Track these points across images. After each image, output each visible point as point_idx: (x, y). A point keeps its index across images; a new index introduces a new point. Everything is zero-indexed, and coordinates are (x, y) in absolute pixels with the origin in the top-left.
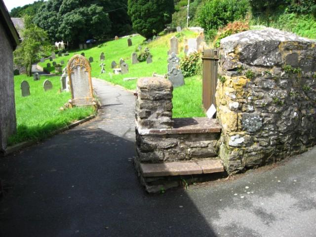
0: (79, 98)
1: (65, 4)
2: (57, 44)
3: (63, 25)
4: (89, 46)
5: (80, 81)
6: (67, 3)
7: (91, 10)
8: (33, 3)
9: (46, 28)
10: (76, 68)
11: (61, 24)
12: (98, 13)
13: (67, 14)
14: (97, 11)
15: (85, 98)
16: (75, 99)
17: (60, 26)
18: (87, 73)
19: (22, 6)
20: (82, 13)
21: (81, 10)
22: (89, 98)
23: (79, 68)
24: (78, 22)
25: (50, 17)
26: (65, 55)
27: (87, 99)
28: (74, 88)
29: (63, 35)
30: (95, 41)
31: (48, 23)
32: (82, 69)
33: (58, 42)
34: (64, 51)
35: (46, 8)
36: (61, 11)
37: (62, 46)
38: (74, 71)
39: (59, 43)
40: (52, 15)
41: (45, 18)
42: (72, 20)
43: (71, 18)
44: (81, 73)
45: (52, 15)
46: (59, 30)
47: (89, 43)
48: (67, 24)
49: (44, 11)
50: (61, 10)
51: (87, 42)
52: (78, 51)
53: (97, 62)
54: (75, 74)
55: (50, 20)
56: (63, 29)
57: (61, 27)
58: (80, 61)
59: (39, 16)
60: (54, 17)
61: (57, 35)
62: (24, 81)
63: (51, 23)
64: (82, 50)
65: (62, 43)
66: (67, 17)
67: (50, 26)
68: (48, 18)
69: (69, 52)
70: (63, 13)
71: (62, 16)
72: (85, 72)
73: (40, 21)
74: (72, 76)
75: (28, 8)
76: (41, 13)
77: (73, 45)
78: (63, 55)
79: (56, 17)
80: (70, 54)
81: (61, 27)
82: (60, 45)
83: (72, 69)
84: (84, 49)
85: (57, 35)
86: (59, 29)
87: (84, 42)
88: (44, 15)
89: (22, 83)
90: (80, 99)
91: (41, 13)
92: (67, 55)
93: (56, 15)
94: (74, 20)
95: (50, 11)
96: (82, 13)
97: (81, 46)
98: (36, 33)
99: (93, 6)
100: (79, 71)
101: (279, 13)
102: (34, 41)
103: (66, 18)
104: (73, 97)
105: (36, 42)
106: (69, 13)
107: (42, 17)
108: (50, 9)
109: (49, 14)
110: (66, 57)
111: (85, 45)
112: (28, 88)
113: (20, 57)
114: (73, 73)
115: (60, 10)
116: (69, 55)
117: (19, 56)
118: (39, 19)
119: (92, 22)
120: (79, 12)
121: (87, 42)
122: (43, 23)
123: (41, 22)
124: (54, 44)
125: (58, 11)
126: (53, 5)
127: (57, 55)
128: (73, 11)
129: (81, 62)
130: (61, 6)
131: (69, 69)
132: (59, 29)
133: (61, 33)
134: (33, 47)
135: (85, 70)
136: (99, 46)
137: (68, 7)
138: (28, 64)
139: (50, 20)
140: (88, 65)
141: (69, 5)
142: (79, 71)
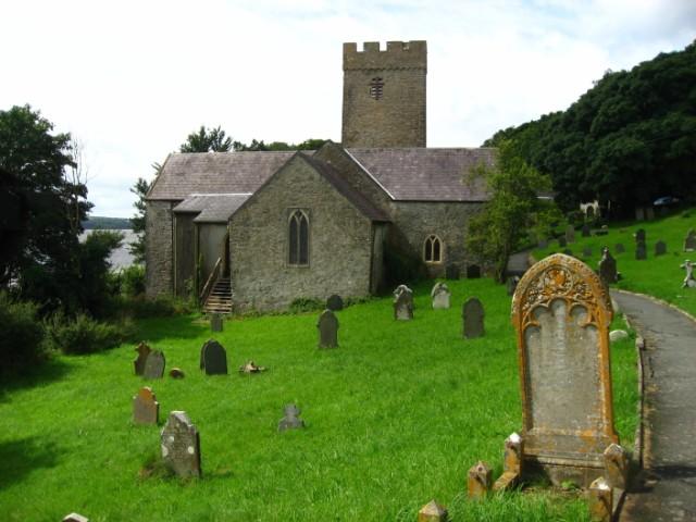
0: (555, 430)
1: (605, 114)
2: (584, 207)
3: (597, 163)
4: (660, 214)
5: (560, 363)
6: (610, 112)
7: (669, 125)
8: (539, 118)
9: (558, 169)
10: (550, 310)
11: (594, 160)
12: (688, 133)
13: (608, 137)
14: (684, 128)
15: (578, 433)
16: (537, 430)
17: (589, 165)
18: (592, 333)
19: (517, 125)
20: (644, 134)
21: (644, 126)
22: (592, 434)
23: (561, 311)
24: (635, 155)
25: (568, 145)
26: (598, 234)
27: (586, 440)
28: (534, 386)
29: (595, 187)
30: (675, 200)
31: (563, 157)
32: (571, 313)
33: (585, 203)
34: (597, 225)
35: (560, 126)
36: (594, 132)
37: (595, 212)
38: (542, 320)
39: (589, 204)
40: (573, 141)
41: (558, 148)
42: (620, 151)
43: (617, 147)
44: (569, 329)
45: (573, 141)
46: (588, 175)
47: (660, 206)
48: (607, 159)
49: (556, 132)
50: (595, 128)
51: (656, 203)
52: (630, 225)
53: (676, 254)
54: (544, 331)
55: (567, 151)
56: (596, 171)
57: (593, 167)
58: (565, 281)
59: (545, 143)
60: (577, 145)
61: (581, 187)
62: (472, 300)
63: (570, 157)
64: (641, 222)
65: (595, 205)
66: (608, 144)
67: (568, 165)
68: (564, 147)
69: (609, 226)
70: (599, 135)
71: (597, 144)
72: (586, 327)
73: (545, 154)
74: (532, 337)
75: (527, 131)
76: (548, 137)
77: (619, 212)
78: (593, 232)
79: (583, 145)
80: (610, 231)
81: (593, 167)
82: (590, 209)
83: (534, 314)
84: (646, 219)
85: (581, 187)
86: (588, 171)
87: (648, 203)
88: (556, 141)
89: (466, 305)
90: (557, 436)
91: (548, 137)
92: (602, 234)
93: (582, 141)
94: (625, 152)
95: (568, 132)
96: (644, 134)
97: (640, 214)
98: (524, 181)
99: (673, 117)
100: (560, 323)
101: (101, 277)
102: (516, 198)
103: (605, 147)
104: (529, 424)
105: (520, 201)
106: (612, 134)
107: (549, 146)
108: (570, 128)
109: (566, 138)
110: (600, 237)
111: (651, 213)
112: (481, 318)
113: (483, 237)
114: (538, 328)
115: (592, 129)
116: (606, 233)
117: (481, 234)
118: (544, 150)
119: (668, 155)
120: (638, 132)
121: (656, 203)
122: (552, 160)
123: (548, 158)
124: (579, 208)
125: (587, 132)
126: (578, 118)
127: (579, 234)
128: (623, 129)
129: (570, 286)
130: (595, 119)
131: (521, 312)
132: (588, 171)
133: (592, 180)
134: (510, 213)
135: (584, 319)
136: (684, 212)
137: (611, 120)
138: (499, 253)
139: (567, 151)
140: (601, 303)
141: (614, 115)
142: (560, 323)
